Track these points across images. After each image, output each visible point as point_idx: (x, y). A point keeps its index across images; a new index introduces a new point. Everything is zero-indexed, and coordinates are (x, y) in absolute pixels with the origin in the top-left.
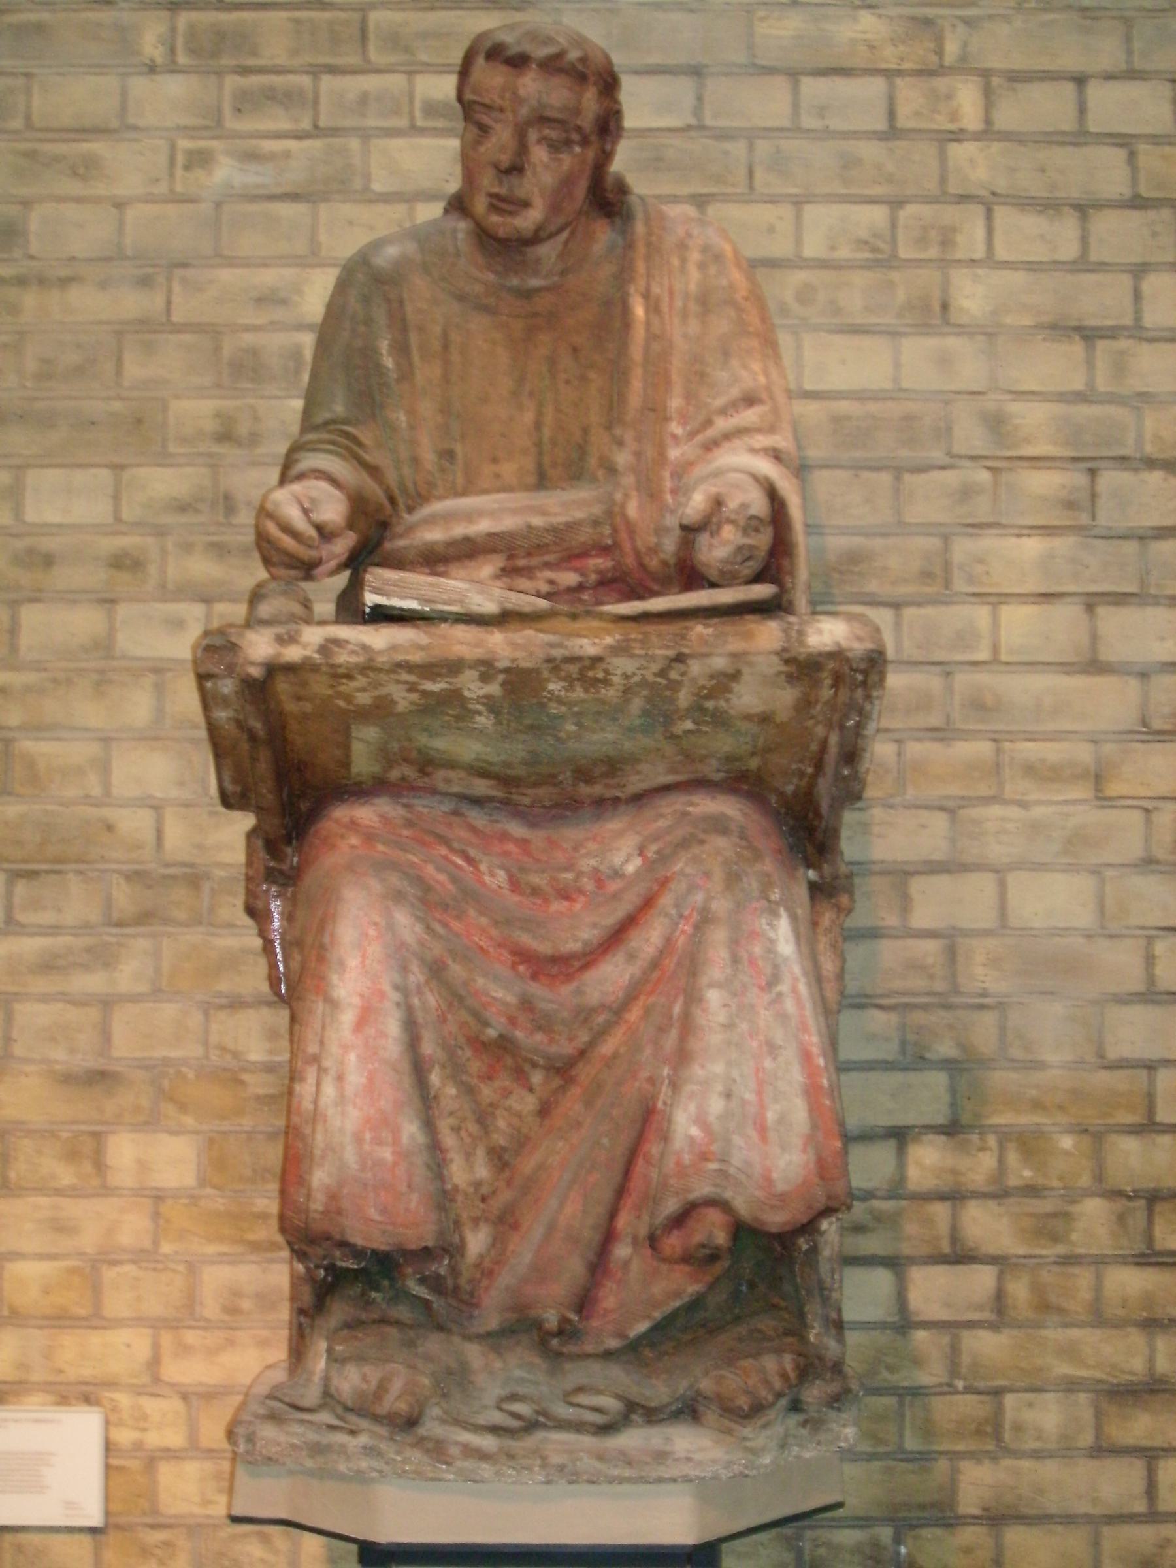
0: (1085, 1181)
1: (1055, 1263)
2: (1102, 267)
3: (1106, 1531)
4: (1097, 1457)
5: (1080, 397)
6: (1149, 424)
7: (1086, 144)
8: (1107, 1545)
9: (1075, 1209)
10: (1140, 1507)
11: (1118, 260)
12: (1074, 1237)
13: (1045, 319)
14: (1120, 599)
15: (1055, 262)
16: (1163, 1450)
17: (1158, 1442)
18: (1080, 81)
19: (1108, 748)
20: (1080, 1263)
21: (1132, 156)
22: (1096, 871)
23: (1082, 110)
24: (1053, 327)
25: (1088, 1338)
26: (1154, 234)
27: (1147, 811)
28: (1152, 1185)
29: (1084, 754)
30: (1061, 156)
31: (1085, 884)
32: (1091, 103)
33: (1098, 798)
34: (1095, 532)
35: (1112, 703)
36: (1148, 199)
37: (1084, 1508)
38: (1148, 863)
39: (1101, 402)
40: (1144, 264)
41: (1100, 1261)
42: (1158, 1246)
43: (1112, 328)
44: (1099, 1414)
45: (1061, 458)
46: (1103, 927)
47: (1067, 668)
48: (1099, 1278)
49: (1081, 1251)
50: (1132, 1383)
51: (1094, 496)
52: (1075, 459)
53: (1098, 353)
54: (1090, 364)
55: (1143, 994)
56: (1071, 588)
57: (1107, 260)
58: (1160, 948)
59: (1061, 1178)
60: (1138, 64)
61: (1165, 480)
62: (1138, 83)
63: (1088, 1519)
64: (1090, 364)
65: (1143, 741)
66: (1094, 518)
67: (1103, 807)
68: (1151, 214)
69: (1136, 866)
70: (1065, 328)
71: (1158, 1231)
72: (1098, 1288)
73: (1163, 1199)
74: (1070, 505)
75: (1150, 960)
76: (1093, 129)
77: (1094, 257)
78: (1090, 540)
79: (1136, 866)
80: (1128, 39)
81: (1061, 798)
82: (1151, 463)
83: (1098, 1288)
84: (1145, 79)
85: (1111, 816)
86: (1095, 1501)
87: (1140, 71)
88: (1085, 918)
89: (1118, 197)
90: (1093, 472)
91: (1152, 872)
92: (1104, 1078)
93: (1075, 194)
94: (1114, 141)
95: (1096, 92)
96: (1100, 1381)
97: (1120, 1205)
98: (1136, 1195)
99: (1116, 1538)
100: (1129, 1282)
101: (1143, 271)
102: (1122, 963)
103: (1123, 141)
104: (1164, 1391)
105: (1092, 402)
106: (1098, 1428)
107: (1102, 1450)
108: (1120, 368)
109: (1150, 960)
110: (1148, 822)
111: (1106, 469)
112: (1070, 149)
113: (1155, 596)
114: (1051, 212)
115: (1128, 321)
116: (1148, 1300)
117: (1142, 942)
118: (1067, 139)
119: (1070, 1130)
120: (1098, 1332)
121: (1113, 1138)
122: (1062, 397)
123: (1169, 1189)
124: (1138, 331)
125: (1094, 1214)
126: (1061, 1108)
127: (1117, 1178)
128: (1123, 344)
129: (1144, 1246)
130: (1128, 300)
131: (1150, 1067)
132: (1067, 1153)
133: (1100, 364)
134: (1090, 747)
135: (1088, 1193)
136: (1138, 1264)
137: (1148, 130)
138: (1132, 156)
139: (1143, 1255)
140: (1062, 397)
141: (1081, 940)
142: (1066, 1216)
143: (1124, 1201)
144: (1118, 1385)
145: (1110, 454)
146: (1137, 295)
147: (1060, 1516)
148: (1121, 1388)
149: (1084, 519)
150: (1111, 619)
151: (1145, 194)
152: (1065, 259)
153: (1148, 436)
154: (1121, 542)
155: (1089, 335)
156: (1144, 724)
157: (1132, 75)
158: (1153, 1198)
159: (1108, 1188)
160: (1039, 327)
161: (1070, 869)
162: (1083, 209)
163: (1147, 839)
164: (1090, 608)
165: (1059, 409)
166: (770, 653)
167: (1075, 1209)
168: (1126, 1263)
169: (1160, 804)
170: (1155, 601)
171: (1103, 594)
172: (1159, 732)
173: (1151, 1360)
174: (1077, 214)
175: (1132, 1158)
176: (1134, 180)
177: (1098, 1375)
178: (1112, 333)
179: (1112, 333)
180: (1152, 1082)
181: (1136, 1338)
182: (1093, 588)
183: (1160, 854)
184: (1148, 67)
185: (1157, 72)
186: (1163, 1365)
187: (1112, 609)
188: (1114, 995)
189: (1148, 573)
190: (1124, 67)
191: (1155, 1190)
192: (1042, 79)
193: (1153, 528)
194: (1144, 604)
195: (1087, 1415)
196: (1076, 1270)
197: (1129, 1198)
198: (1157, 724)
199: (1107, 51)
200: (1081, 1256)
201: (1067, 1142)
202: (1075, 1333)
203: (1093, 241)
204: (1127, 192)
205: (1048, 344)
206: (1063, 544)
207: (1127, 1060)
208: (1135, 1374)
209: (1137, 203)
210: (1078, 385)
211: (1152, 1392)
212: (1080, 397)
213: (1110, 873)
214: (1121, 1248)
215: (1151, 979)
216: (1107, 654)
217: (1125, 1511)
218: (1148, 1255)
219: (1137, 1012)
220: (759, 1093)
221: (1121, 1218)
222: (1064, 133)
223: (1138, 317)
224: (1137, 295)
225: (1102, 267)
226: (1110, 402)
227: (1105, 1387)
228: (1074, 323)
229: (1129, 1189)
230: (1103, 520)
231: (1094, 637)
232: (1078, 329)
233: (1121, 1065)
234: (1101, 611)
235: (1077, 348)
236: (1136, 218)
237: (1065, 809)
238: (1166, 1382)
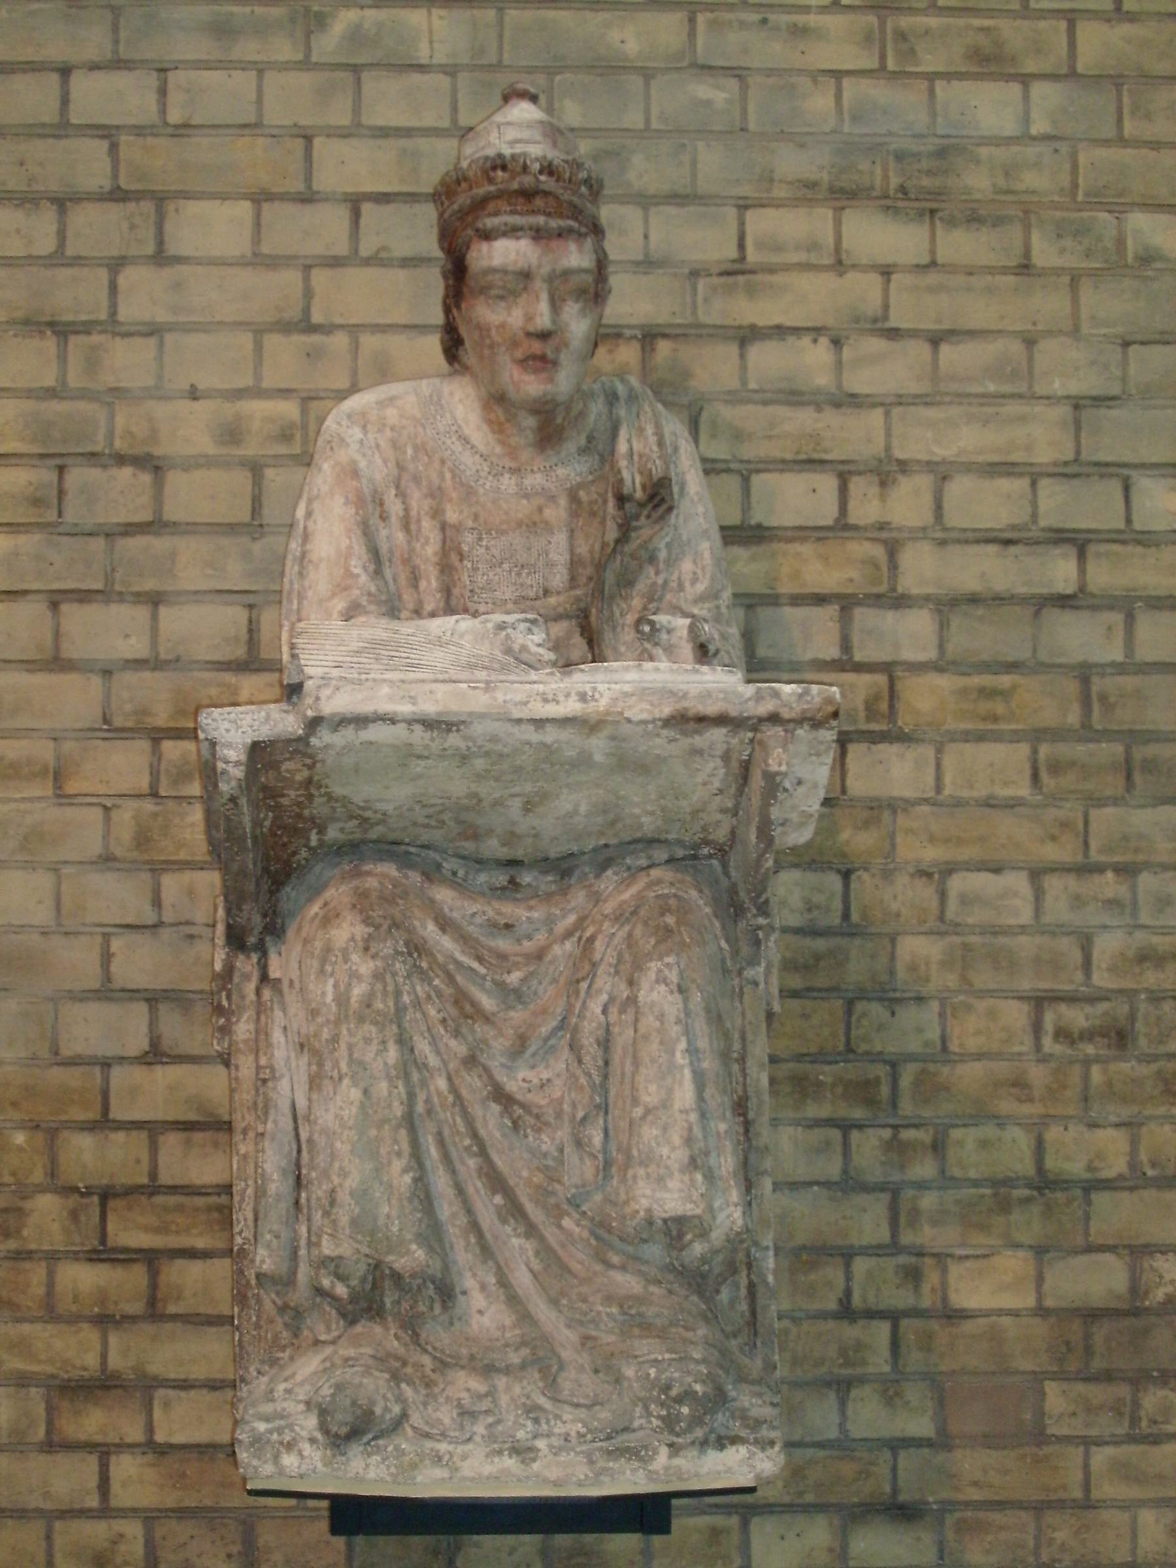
0: (38, 1176)
1: (6, 1258)
2: (78, 261)
3: (58, 1525)
4: (50, 1452)
5: (51, 393)
6: (120, 421)
7: (67, 136)
8: (58, 1541)
9: (28, 1205)
10: (93, 1502)
11: (96, 254)
12: (25, 1233)
13: (19, 314)
14: (84, 596)
15: (30, 257)
16: (115, 1445)
17: (112, 1438)
18: (65, 71)
19: (68, 746)
20: (30, 1259)
21: (114, 148)
22: (54, 869)
23: (65, 101)
24: (27, 322)
25: (40, 1333)
26: (133, 227)
27: (106, 809)
28: (105, 1182)
29: (44, 751)
30: (39, 148)
31: (44, 881)
32: (74, 95)
33: (59, 796)
34: (61, 529)
35: (75, 700)
36: (127, 192)
37: (35, 1501)
38: (107, 860)
39: (72, 398)
40: (124, 257)
41: (53, 1257)
42: (110, 1243)
43: (84, 323)
44: (50, 1409)
45: (28, 455)
46: (59, 925)
47: (30, 665)
48: (51, 1274)
49: (33, 1246)
50: (82, 1378)
51: (61, 493)
52: (43, 456)
53: (71, 347)
54: (63, 358)
55: (96, 991)
56: (35, 586)
57: (83, 254)
58: (116, 945)
59: (13, 1174)
60: (124, 53)
61: (134, 475)
62: (124, 73)
63: (40, 1512)
64: (63, 358)
65: (104, 739)
66: (60, 514)
67: (61, 805)
68: (131, 206)
69: (92, 863)
70: (38, 323)
71: (110, 1227)
72: (51, 1284)
73: (116, 1196)
74: (37, 502)
75: (107, 957)
76: (74, 121)
77: (70, 251)
78: (55, 537)
79: (92, 863)
80: (115, 28)
81: (18, 796)
82: (121, 460)
83: (51, 1284)
84: (130, 69)
85: (70, 812)
86: (46, 1495)
87: (128, 61)
88: (43, 915)
89: (98, 190)
90: (61, 469)
91: (109, 869)
92: (57, 1075)
93: (54, 187)
94: (100, 133)
95: (80, 83)
96: (53, 1377)
97: (73, 1201)
98: (89, 1193)
99: (69, 1533)
100: (83, 1279)
101: (122, 265)
102: (78, 960)
103: (107, 133)
104: (116, 1387)
105: (62, 398)
106: (50, 1423)
107: (53, 1445)
108: (92, 364)
109: (107, 957)
110: (107, 820)
111: (74, 466)
112: (50, 141)
113: (121, 593)
114: (28, 206)
115: (103, 316)
116: (102, 1297)
117: (99, 939)
118: (48, 131)
119: (21, 1126)
120: (49, 1327)
121: (65, 1134)
122: (30, 394)
123: (122, 1185)
124: (113, 326)
125: (47, 1209)
126: (15, 1104)
127: (71, 1173)
128: (95, 339)
129: (96, 1243)
130: (104, 294)
131: (106, 1064)
132: (20, 1149)
133: (71, 358)
134: (51, 744)
135: (41, 1189)
136: (91, 1260)
137: (132, 121)
138: (114, 148)
139: (95, 1251)
140: (30, 394)
141: (36, 937)
142: (20, 1212)
143: (76, 1196)
144: (69, 1380)
145: (81, 450)
146: (113, 288)
147: (12, 1511)
148: (73, 1384)
149: (51, 516)
150: (74, 616)
151: (124, 186)
152: (43, 253)
153: (118, 431)
154: (87, 538)
155: (62, 331)
156: (105, 720)
157: (118, 64)
158: (106, 1195)
159: (60, 1184)
160: (12, 322)
161: (30, 866)
162: (62, 203)
163: (106, 835)
164: (54, 606)
165: (29, 405)
166: (923, 741)
167: (28, 1205)
168: (77, 1259)
169: (118, 801)
170: (121, 598)
171: (72, 591)
172: (122, 730)
173: (104, 1356)
174: (55, 207)
175: (86, 1154)
176: (115, 176)
177: (50, 1369)
178: (86, 328)
179: (86, 328)
180: (106, 1080)
181: (90, 1334)
182: (55, 586)
183: (118, 852)
184: (137, 56)
185: (142, 61)
186: (115, 1361)
187: (75, 606)
188: (70, 991)
189: (113, 570)
190: (109, 56)
191: (108, 1186)
192: (25, 71)
193: (118, 524)
194: (108, 602)
195: (41, 1409)
196: (27, 1265)
197: (82, 1195)
198: (118, 722)
199: (93, 40)
200: (31, 1252)
201: (20, 1138)
202: (26, 1328)
203: (70, 234)
204: (107, 184)
205: (19, 339)
206: (28, 542)
207: (79, 1056)
208: (86, 1369)
209: (117, 195)
210: (49, 381)
211: (107, 1388)
212: (51, 393)
213: (66, 870)
214: (74, 1244)
215: (108, 977)
216: (69, 651)
217: (77, 1506)
218: (99, 1252)
219: (94, 1009)
220: (1037, 1538)
221: (74, 1215)
222: (44, 125)
223: (113, 313)
224: (113, 288)
225: (78, 261)
226: (82, 398)
227: (57, 1382)
228: (49, 319)
229: (81, 1185)
230: (70, 517)
231: (57, 634)
232: (51, 324)
233: (75, 1062)
234: (65, 608)
235: (50, 344)
236: (114, 212)
237: (22, 806)
238: (118, 1378)
